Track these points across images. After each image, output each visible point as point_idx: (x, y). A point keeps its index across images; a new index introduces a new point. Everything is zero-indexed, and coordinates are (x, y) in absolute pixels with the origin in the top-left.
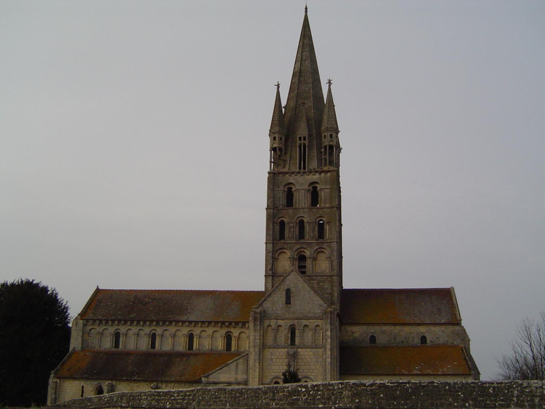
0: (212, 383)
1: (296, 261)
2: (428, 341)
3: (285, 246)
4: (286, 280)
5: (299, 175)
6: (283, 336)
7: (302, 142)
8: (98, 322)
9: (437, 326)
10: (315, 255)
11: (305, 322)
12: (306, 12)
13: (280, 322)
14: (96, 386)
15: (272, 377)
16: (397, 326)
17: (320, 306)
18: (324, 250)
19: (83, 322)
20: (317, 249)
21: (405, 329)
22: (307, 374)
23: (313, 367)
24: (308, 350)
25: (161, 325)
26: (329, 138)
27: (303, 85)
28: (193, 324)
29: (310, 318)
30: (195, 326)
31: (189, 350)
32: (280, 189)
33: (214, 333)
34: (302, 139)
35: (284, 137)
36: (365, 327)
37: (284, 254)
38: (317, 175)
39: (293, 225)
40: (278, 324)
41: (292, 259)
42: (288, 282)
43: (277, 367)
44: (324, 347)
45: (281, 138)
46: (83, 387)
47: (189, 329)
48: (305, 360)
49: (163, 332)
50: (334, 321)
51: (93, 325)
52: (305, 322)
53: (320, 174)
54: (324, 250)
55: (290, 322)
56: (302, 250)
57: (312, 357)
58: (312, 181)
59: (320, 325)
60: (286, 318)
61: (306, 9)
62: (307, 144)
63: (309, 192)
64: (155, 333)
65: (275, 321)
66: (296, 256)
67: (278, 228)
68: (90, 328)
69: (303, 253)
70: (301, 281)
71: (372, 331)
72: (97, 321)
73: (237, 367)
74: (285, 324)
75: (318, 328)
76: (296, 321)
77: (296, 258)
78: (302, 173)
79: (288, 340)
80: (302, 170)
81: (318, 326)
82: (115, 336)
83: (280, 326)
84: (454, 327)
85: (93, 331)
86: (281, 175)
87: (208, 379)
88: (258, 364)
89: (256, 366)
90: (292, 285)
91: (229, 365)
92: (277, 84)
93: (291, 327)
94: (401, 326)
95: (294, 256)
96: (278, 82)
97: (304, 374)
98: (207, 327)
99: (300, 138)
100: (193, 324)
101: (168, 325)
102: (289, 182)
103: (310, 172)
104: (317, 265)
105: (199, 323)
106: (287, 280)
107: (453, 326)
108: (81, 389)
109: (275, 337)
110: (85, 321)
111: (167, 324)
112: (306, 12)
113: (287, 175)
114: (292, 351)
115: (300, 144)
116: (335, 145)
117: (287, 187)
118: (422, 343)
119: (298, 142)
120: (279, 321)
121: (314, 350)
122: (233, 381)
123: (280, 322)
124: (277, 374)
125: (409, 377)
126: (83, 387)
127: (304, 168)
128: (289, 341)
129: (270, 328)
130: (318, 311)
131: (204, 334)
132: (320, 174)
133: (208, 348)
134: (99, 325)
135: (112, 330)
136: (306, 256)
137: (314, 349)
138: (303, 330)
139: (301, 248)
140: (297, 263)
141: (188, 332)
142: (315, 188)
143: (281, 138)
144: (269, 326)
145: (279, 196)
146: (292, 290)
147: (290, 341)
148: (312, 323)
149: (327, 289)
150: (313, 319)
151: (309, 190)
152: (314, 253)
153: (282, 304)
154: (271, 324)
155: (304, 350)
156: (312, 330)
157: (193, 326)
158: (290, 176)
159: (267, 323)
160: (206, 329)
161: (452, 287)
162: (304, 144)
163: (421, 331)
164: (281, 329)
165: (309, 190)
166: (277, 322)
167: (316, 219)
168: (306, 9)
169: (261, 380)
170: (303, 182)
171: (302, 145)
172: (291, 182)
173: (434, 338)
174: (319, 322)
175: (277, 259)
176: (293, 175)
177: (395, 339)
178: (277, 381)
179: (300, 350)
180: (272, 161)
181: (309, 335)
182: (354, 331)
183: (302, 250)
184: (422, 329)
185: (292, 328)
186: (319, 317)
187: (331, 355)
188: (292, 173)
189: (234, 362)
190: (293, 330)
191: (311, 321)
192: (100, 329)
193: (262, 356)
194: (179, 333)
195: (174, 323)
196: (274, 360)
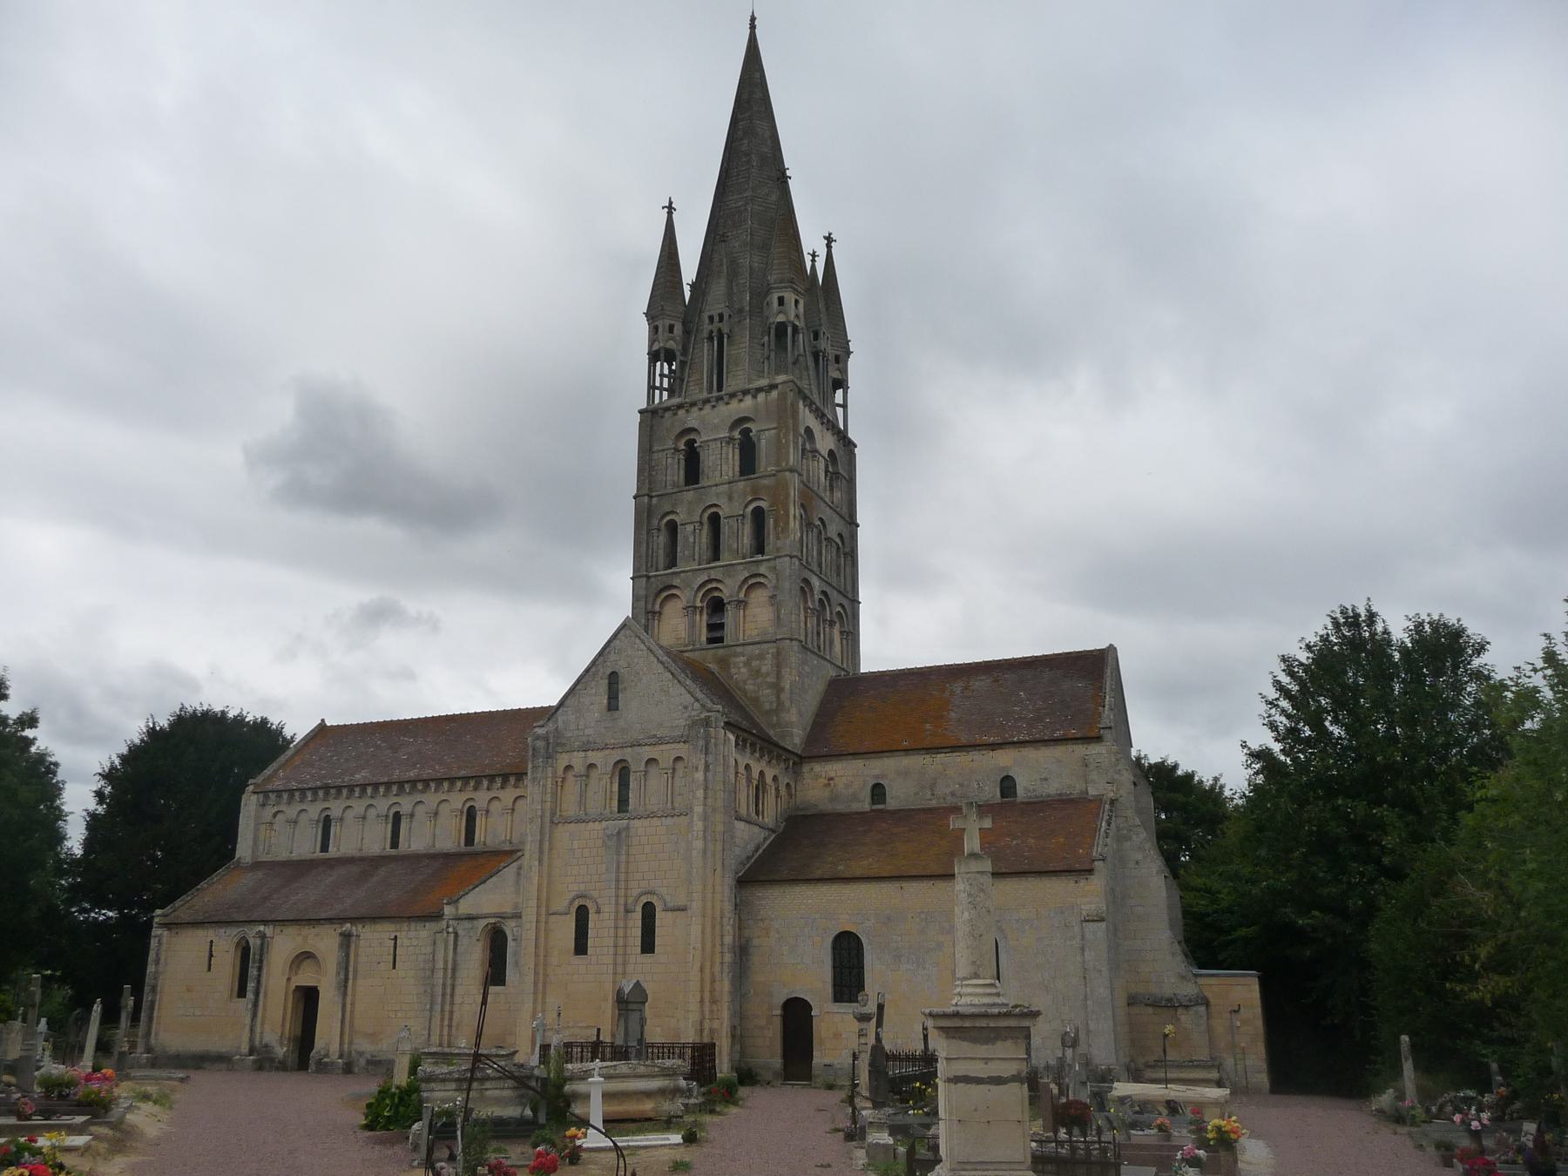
0: (466, 919)
1: (701, 612)
2: (1020, 791)
3: (676, 582)
4: (609, 653)
5: (708, 407)
6: (602, 788)
7: (716, 325)
8: (285, 796)
9: (1043, 748)
10: (742, 595)
11: (648, 752)
12: (753, 27)
13: (593, 757)
14: (235, 940)
15: (574, 894)
16: (939, 756)
18: (762, 580)
19: (258, 800)
20: (746, 579)
21: (959, 759)
24: (656, 821)
25: (408, 791)
27: (731, 198)
28: (472, 783)
30: (476, 789)
31: (466, 845)
32: (666, 447)
33: (518, 800)
34: (716, 319)
36: (858, 764)
38: (749, 401)
39: (693, 527)
40: (589, 762)
41: (691, 609)
46: (212, 942)
47: (465, 796)
49: (414, 806)
50: (716, 745)
51: (278, 804)
52: (648, 752)
53: (755, 397)
54: (762, 580)
55: (617, 755)
56: (714, 585)
58: (737, 417)
59: (684, 757)
60: (606, 745)
61: (753, 19)
63: (731, 445)
64: (399, 812)
65: (583, 754)
66: (701, 601)
67: (662, 539)
68: (274, 811)
69: (716, 594)
71: (877, 772)
72: (283, 793)
73: (519, 874)
74: (604, 761)
75: (680, 765)
77: (702, 608)
78: (714, 399)
79: (611, 799)
80: (715, 394)
81: (678, 759)
82: (321, 825)
83: (592, 766)
84: (1089, 748)
85: (279, 816)
86: (668, 414)
88: (537, 863)
89: (533, 868)
90: (623, 663)
91: (501, 872)
92: (667, 205)
93: (620, 766)
94: (948, 755)
95: (694, 601)
96: (670, 198)
98: (502, 788)
99: (711, 318)
100: (472, 783)
101: (423, 792)
102: (687, 426)
103: (732, 395)
104: (748, 619)
105: (484, 779)
106: (612, 653)
107: (1086, 746)
109: (582, 795)
110: (261, 796)
111: (420, 788)
112: (753, 27)
113: (681, 412)
115: (711, 332)
117: (683, 441)
118: (1003, 795)
119: (707, 327)
121: (669, 821)
124: (582, 887)
125: (925, 882)
126: (212, 942)
127: (720, 388)
128: (615, 803)
129: (570, 775)
130: (680, 721)
131: (495, 806)
132: (755, 397)
133: (504, 838)
134: (289, 803)
135: (314, 810)
136: (723, 597)
138: (646, 772)
139: (710, 581)
140: (705, 617)
141: (464, 805)
142: (746, 433)
144: (568, 768)
145: (664, 463)
146: (622, 672)
147: (616, 801)
148: (665, 754)
149: (767, 674)
150: (668, 743)
151: (732, 439)
152: (740, 587)
154: (571, 764)
155: (646, 822)
156: (665, 771)
157: (472, 788)
158: (687, 411)
159: (563, 761)
160: (501, 794)
161: (1111, 645)
162: (720, 331)
163: (1001, 765)
164: (594, 774)
165: (732, 439)
167: (746, 506)
168: (753, 19)
169: (544, 902)
170: (716, 421)
172: (691, 426)
173: (1036, 780)
174: (681, 749)
175: (660, 613)
176: (695, 409)
177: (932, 787)
178: (584, 904)
179: (636, 823)
180: (840, 411)
181: (656, 781)
183: (714, 585)
184: (1004, 760)
185: (620, 771)
186: (682, 736)
187: (705, 831)
188: (693, 404)
189: (512, 865)
190: (622, 772)
191: (663, 747)
192: (291, 811)
193: (550, 844)
194: (444, 808)
195: (433, 785)
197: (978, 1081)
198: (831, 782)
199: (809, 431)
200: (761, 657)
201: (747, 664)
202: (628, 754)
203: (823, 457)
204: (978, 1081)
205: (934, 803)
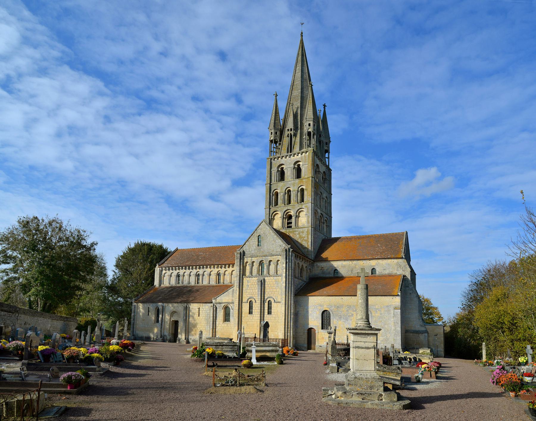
13: (254, 259)
17: (280, 246)
19: (160, 269)
22: (271, 295)
23: (275, 290)
26: (308, 126)
29: (273, 255)
35: (279, 132)
37: (277, 215)
42: (259, 231)
43: (251, 291)
44: (281, 276)
45: (276, 133)
46: (149, 307)
47: (217, 270)
48: (269, 286)
52: (270, 258)
55: (260, 259)
57: (274, 283)
61: (302, 33)
62: (292, 134)
70: (268, 229)
74: (257, 260)
76: (264, 258)
87: (216, 300)
97: (269, 295)
108: (148, 309)
114: (262, 278)
116: (312, 131)
120: (253, 258)
122: (231, 302)
123: (254, 259)
124: (251, 296)
126: (149, 307)
135: (175, 273)
137: (276, 277)
143: (276, 133)
146: (262, 236)
149: (304, 237)
153: (255, 247)
162: (291, 134)
166: (252, 259)
168: (302, 33)
171: (289, 135)
182: (323, 266)
196: (250, 286)
197: (362, 348)
198: (323, 269)
199: (317, 165)
200: (303, 232)
201: (299, 234)
202: (264, 258)
203: (322, 174)
204: (362, 348)
205: (352, 275)
